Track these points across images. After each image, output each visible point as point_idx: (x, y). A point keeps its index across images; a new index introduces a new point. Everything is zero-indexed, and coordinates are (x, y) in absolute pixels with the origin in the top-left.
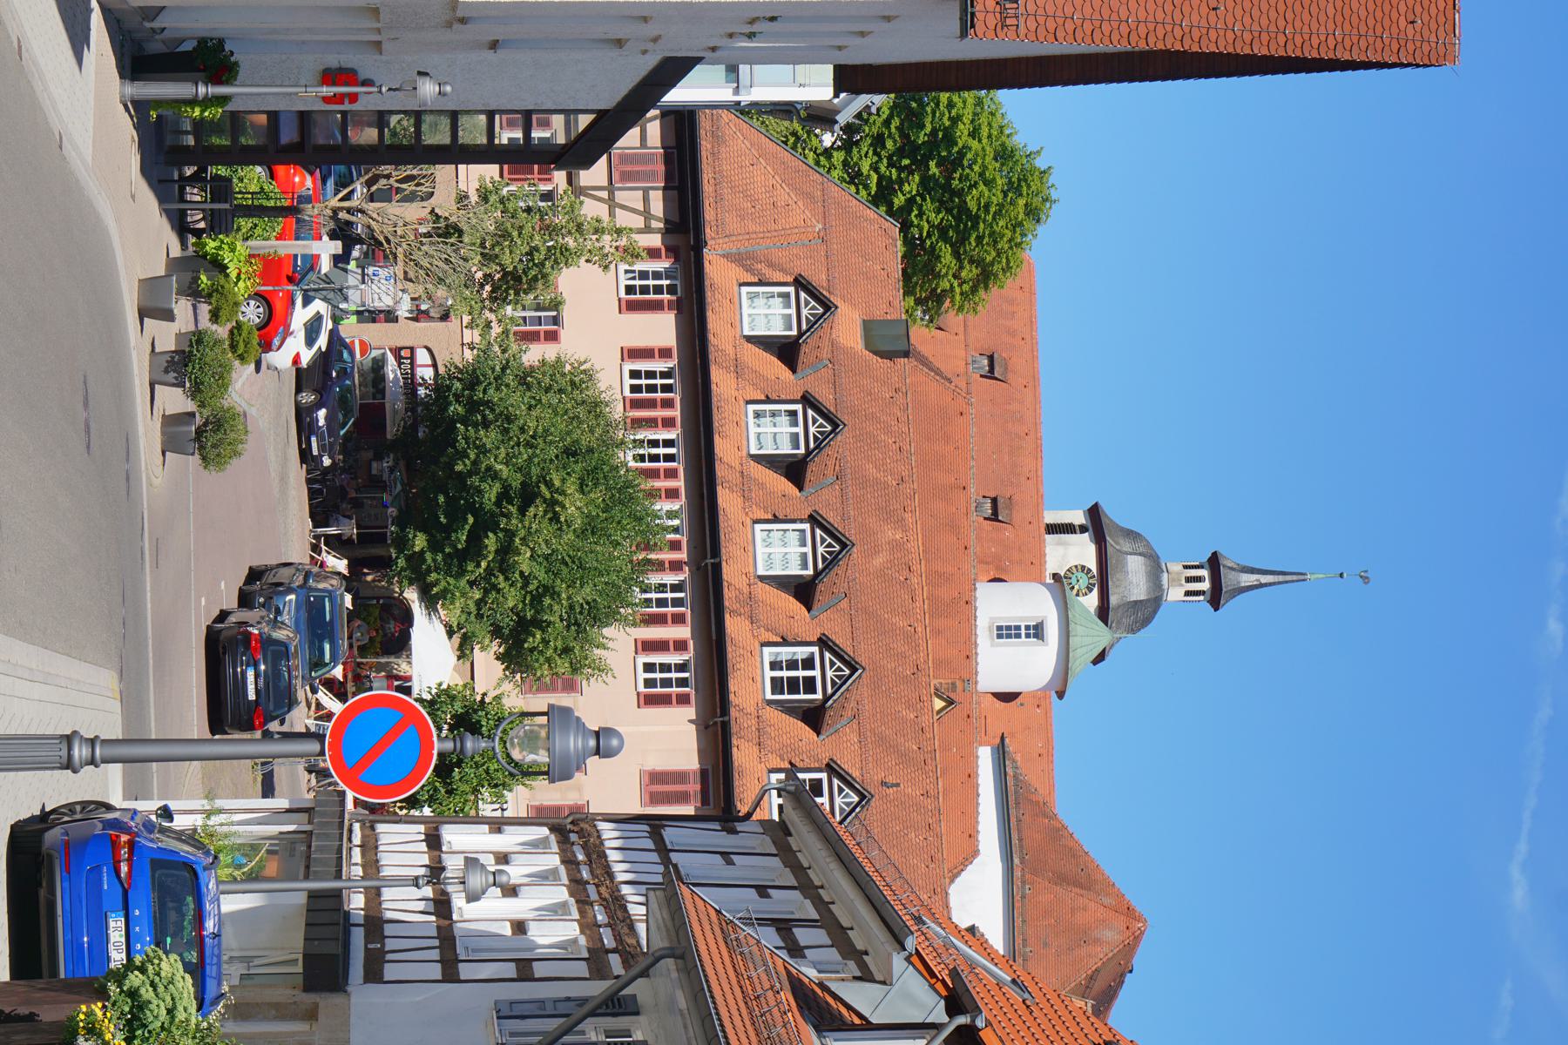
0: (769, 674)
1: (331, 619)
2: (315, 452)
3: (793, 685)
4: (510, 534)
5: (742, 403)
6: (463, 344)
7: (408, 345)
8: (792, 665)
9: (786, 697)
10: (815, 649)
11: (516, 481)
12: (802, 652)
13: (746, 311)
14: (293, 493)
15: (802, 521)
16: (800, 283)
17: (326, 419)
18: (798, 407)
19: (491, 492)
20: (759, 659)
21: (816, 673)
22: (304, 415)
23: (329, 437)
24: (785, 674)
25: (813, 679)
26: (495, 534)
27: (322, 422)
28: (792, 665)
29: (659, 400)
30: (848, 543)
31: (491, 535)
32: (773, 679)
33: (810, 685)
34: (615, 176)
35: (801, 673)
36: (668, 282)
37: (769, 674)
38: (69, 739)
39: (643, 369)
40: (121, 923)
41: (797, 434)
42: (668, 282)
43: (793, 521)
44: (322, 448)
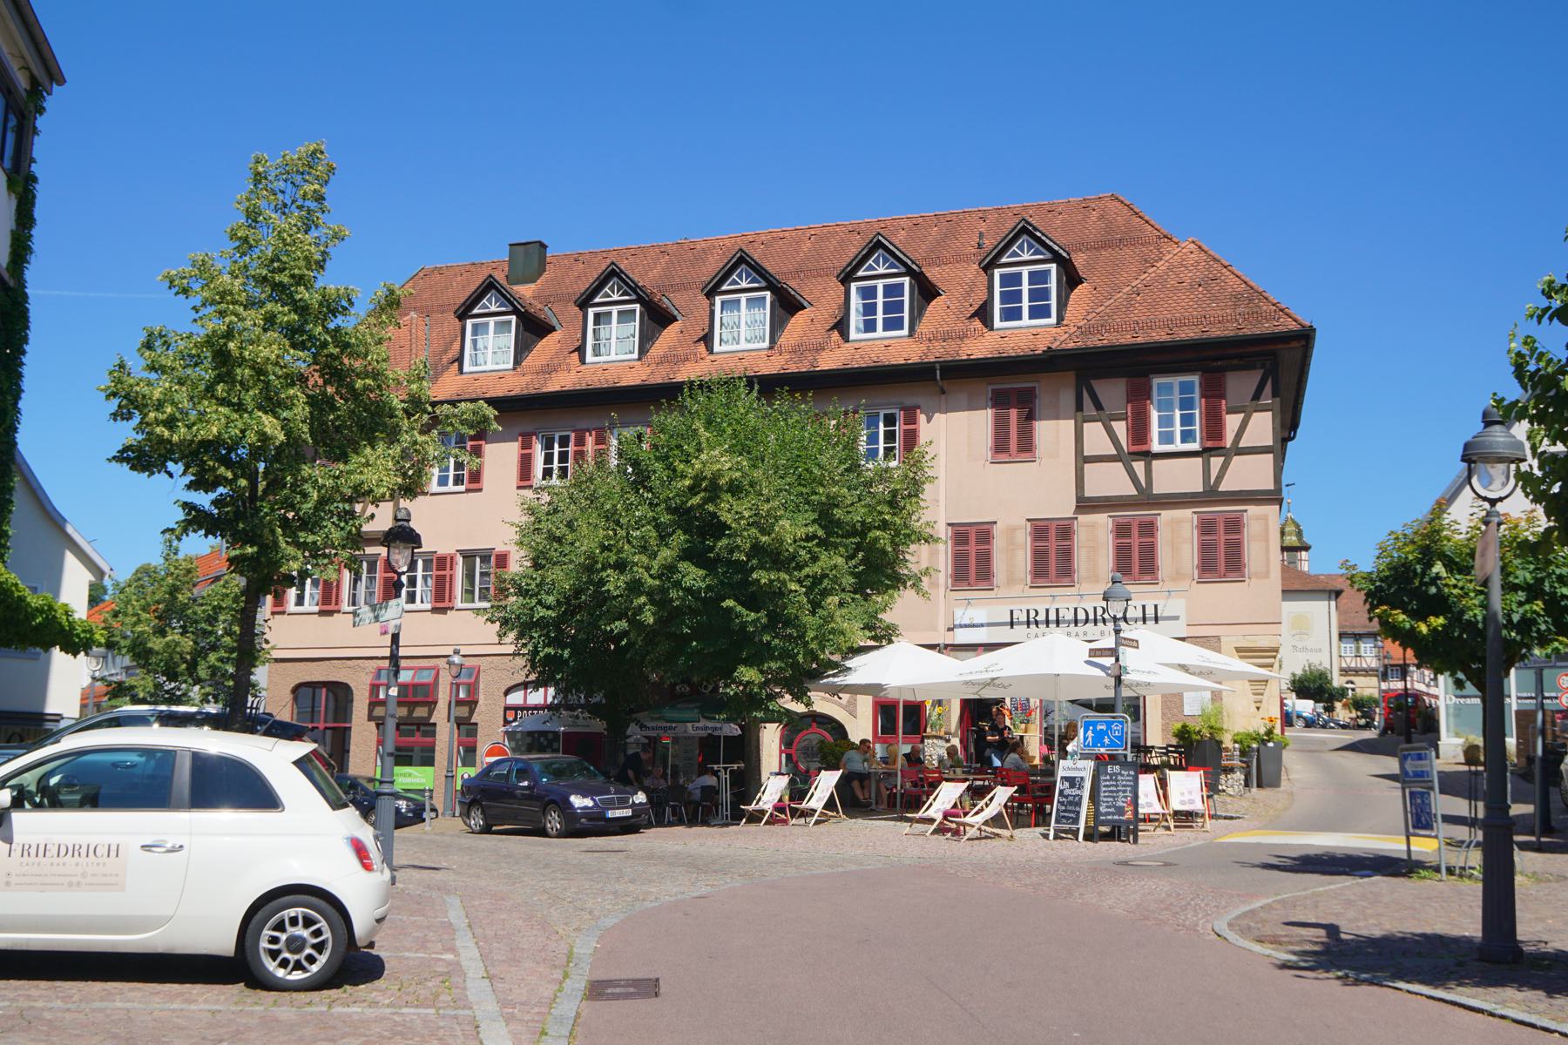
1: (1485, 628)
2: (628, 813)
3: (1039, 295)
4: (757, 549)
5: (584, 367)
6: (500, 644)
7: (502, 713)
10: (854, 286)
11: (679, 539)
12: (856, 302)
14: (165, 989)
15: (712, 304)
17: (584, 796)
18: (591, 312)
19: (693, 575)
20: (863, 343)
21: (880, 284)
22: (578, 826)
23: (609, 793)
24: (880, 316)
25: (886, 287)
26: (753, 569)
27: (588, 802)
28: (869, 309)
29: (576, 448)
30: (738, 255)
31: (755, 576)
33: (1036, 278)
35: (880, 300)
36: (881, 425)
37: (880, 332)
38: (447, 777)
42: (881, 425)
43: (712, 313)
44: (623, 803)
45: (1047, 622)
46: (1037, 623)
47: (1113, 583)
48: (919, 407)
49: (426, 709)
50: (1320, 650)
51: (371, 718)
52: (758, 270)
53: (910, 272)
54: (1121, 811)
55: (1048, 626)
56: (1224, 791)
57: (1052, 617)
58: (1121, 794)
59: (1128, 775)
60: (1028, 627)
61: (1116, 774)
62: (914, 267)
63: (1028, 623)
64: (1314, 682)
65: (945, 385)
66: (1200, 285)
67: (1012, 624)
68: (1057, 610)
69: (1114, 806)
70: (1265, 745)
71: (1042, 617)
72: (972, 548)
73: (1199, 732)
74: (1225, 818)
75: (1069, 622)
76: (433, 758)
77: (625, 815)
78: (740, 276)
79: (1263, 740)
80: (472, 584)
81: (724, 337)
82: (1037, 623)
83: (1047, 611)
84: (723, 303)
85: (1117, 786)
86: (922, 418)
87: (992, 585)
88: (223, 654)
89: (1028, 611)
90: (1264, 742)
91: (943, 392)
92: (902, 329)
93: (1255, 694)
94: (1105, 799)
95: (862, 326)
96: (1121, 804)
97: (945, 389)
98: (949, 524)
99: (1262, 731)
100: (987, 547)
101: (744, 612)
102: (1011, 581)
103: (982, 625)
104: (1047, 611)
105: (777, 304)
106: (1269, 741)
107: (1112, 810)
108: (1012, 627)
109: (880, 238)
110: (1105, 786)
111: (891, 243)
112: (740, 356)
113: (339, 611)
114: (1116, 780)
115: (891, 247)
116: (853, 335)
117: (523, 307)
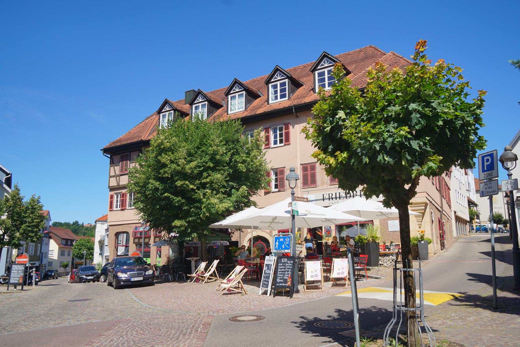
0: (279, 100)
2: (142, 279)
8: (276, 92)
9: (287, 92)
13: (237, 111)
16: (159, 112)
18: (194, 106)
21: (326, 70)
25: (280, 84)
28: (276, 92)
32: (281, 98)
34: (126, 173)
35: (279, 89)
36: (278, 131)
37: (279, 100)
39: (273, 140)
40: (170, 254)
41: (239, 95)
42: (278, 131)
45: (336, 198)
46: (332, 198)
47: (291, 171)
48: (290, 123)
49: (148, 239)
50: (501, 208)
51: (134, 243)
52: (241, 85)
53: (288, 77)
54: (285, 281)
55: (336, 199)
56: (383, 264)
57: (338, 196)
58: (286, 273)
59: (290, 263)
60: (329, 200)
61: (285, 263)
62: (289, 75)
63: (329, 199)
64: (497, 218)
65: (298, 114)
66: (390, 66)
67: (323, 199)
68: (339, 193)
69: (283, 279)
70: (420, 242)
71: (334, 196)
72: (309, 172)
73: (367, 239)
74: (376, 278)
75: (344, 197)
76: (150, 255)
77: (139, 280)
78: (277, 76)
79: (419, 240)
80: (131, 197)
81: (232, 109)
82: (332, 198)
83: (336, 193)
84: (231, 97)
85: (285, 269)
86: (291, 127)
87: (316, 185)
88: (27, 224)
89: (329, 194)
90: (420, 241)
91: (298, 117)
92: (286, 97)
93: (418, 222)
94: (280, 275)
95: (274, 99)
96: (286, 278)
97: (298, 116)
98: (301, 164)
99: (419, 236)
100: (314, 171)
101: (175, 198)
102: (323, 184)
103: (313, 201)
104: (336, 193)
105: (247, 95)
106: (422, 241)
107: (282, 281)
108: (324, 201)
109: (278, 67)
110: (280, 269)
111: (281, 68)
112: (235, 114)
113: (126, 209)
114: (285, 266)
115: (281, 70)
116: (270, 102)
117: (175, 107)
